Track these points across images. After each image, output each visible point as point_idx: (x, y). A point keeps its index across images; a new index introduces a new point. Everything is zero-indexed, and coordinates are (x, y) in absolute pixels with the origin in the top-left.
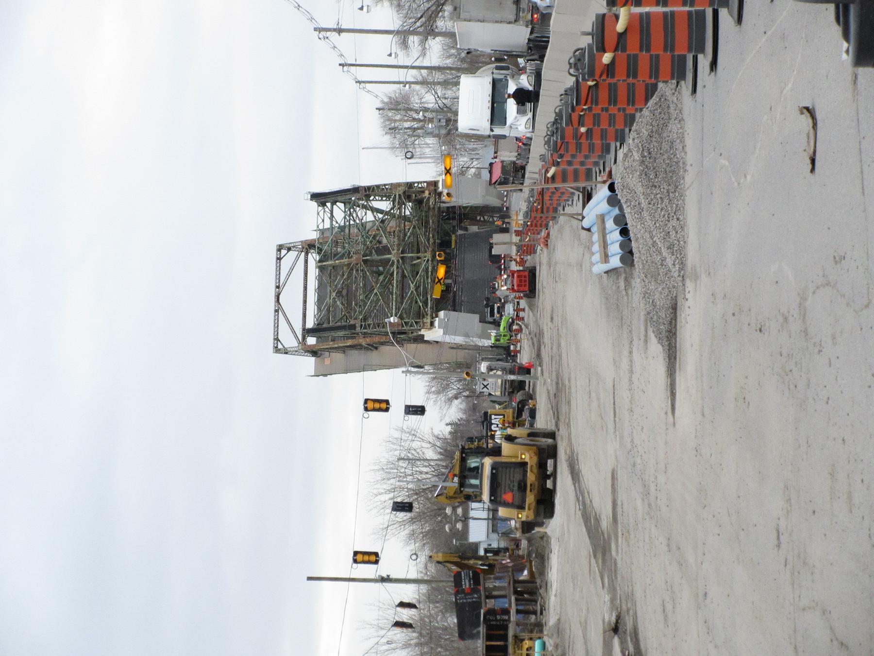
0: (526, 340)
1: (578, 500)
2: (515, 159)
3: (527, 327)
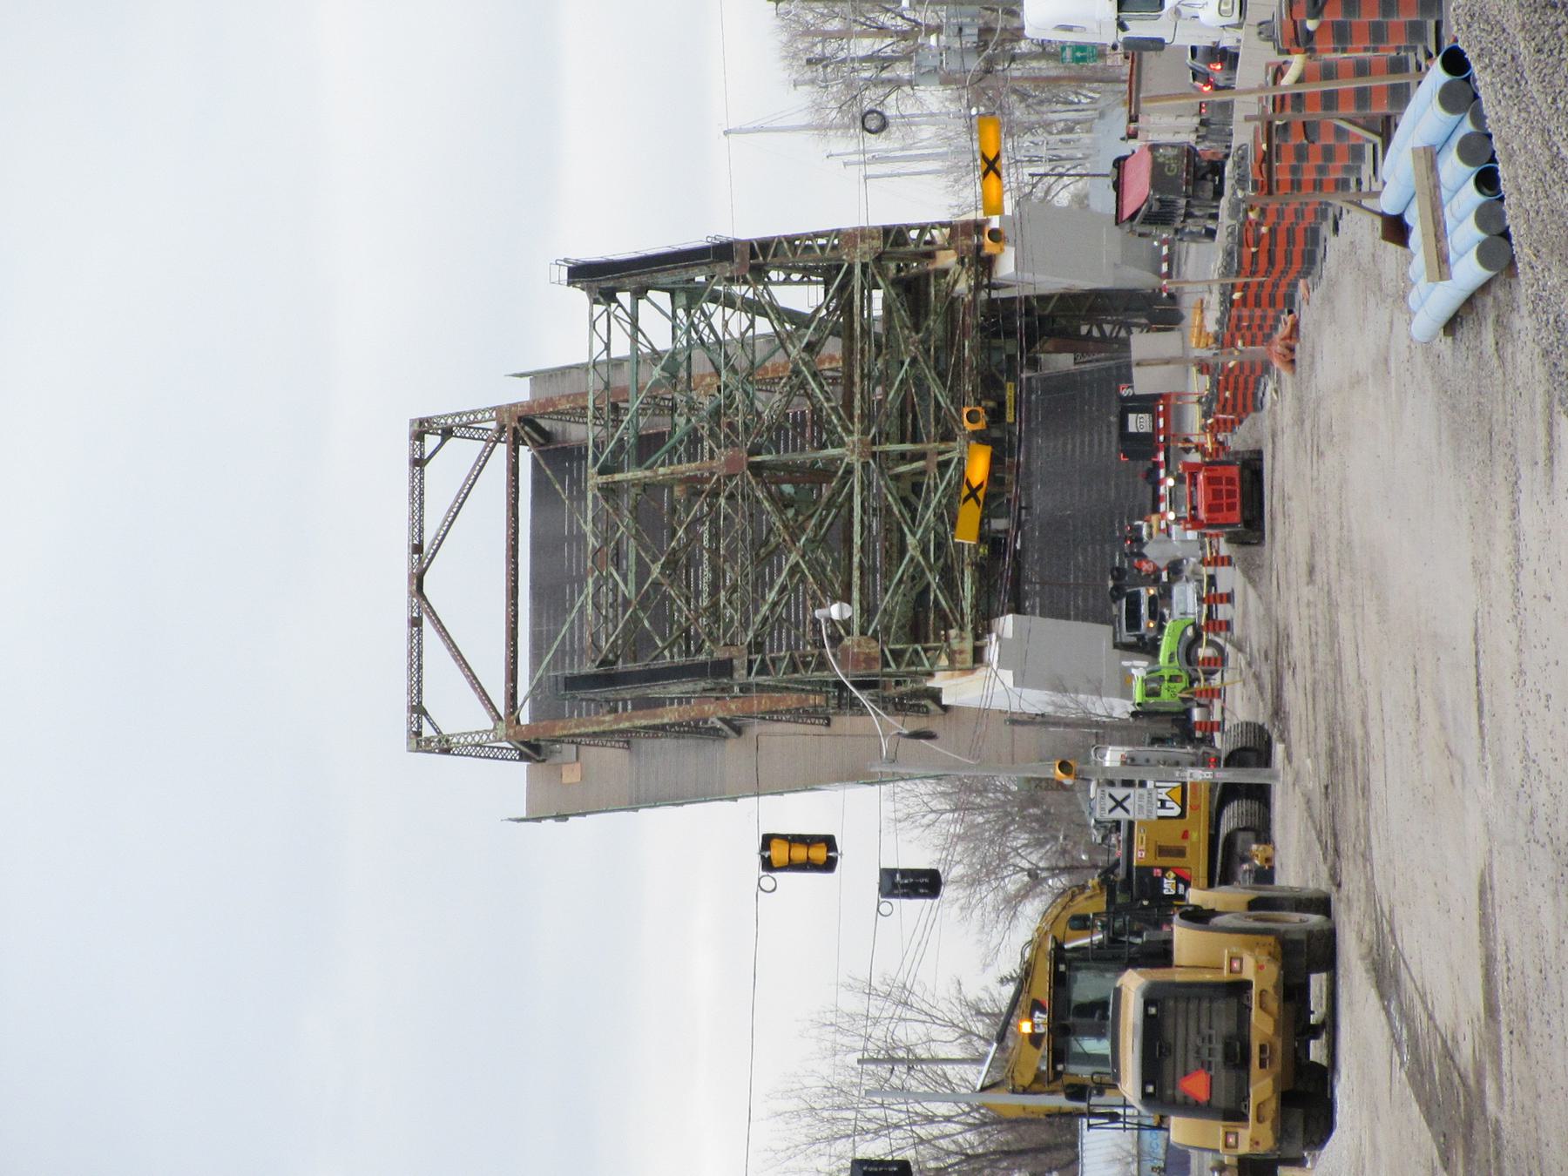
0: (1239, 685)
1: (1397, 1044)
2: (1192, 138)
3: (1239, 648)
